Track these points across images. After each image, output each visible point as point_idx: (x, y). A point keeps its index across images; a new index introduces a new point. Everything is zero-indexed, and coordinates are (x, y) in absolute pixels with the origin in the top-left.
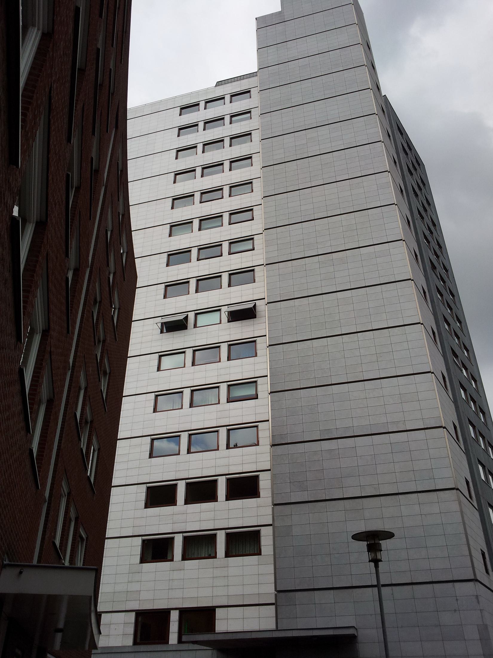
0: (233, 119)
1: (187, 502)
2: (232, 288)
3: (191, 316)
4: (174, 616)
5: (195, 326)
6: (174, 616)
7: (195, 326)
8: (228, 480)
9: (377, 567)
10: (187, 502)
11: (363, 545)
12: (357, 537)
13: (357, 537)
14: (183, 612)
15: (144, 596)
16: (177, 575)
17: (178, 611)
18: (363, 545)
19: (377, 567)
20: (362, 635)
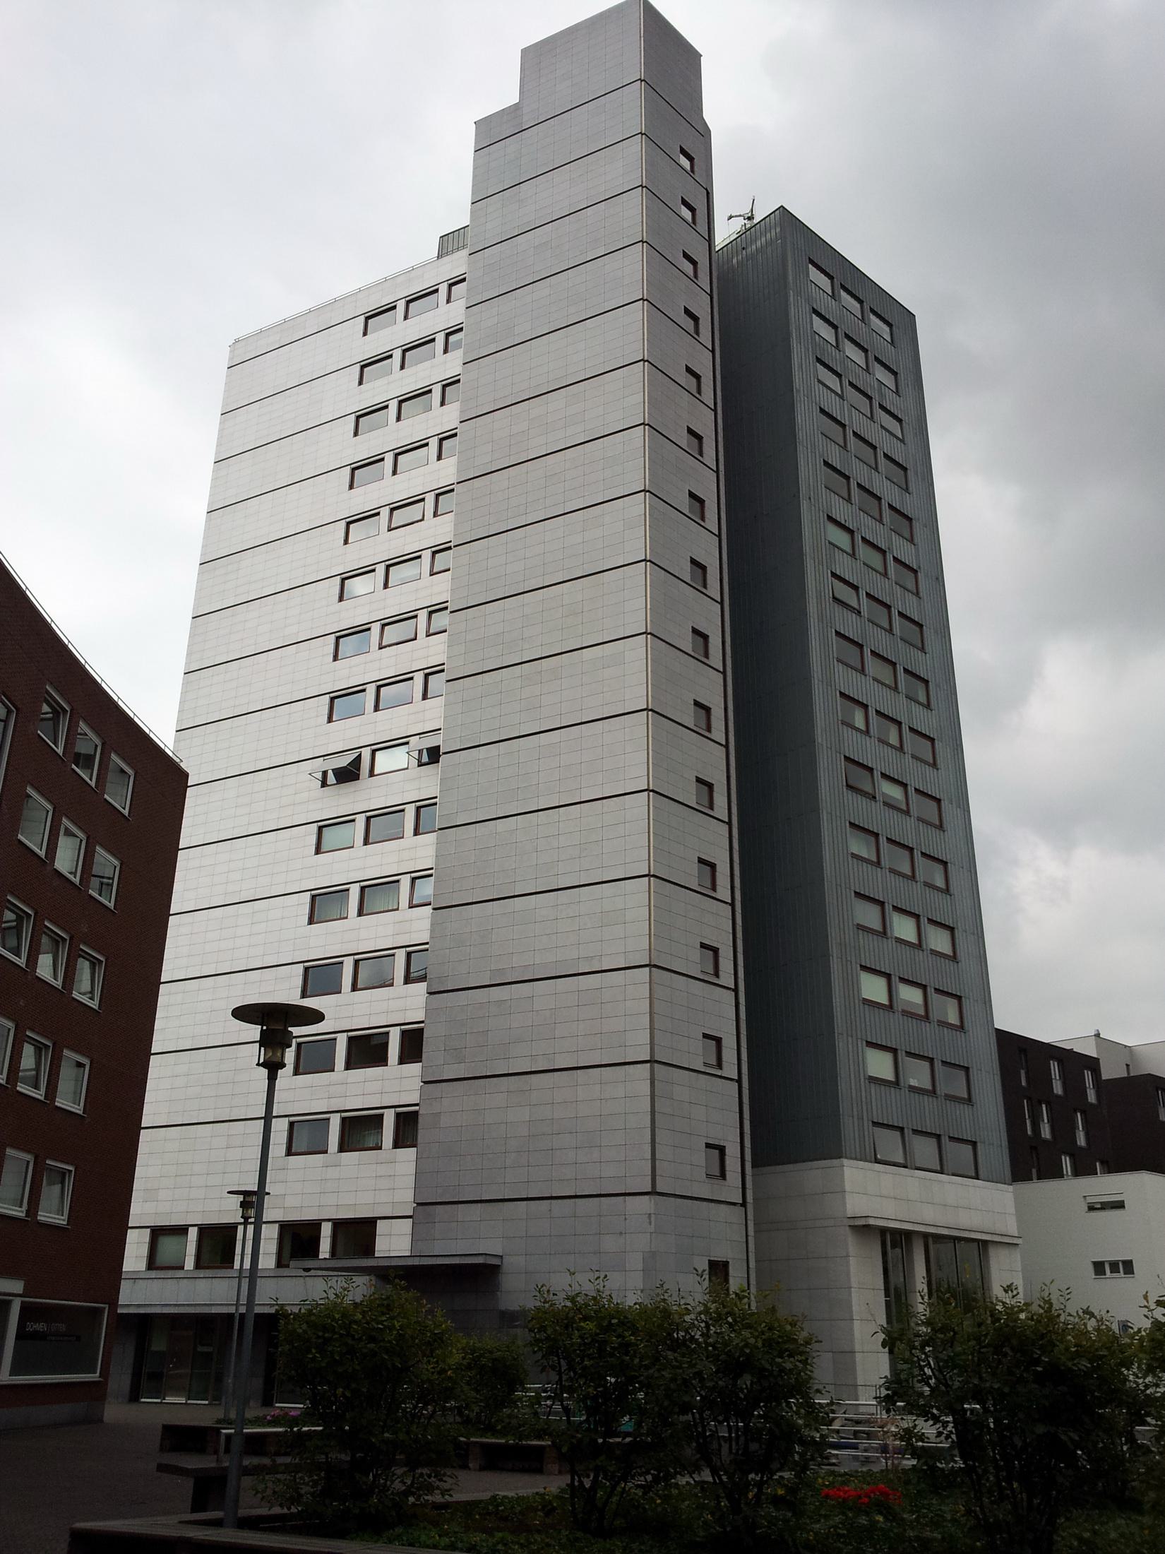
0: (452, 338)
1: (348, 1066)
2: (696, 865)
3: (366, 754)
4: (326, 1230)
5: (372, 774)
6: (326, 1230)
7: (372, 774)
8: (403, 1033)
9: (272, 1078)
10: (348, 1066)
11: (254, 1031)
12: (242, 1013)
13: (242, 1013)
14: (338, 1224)
15: (290, 1202)
16: (332, 1173)
17: (330, 1224)
18: (254, 1031)
19: (272, 1078)
20: (510, 1264)
